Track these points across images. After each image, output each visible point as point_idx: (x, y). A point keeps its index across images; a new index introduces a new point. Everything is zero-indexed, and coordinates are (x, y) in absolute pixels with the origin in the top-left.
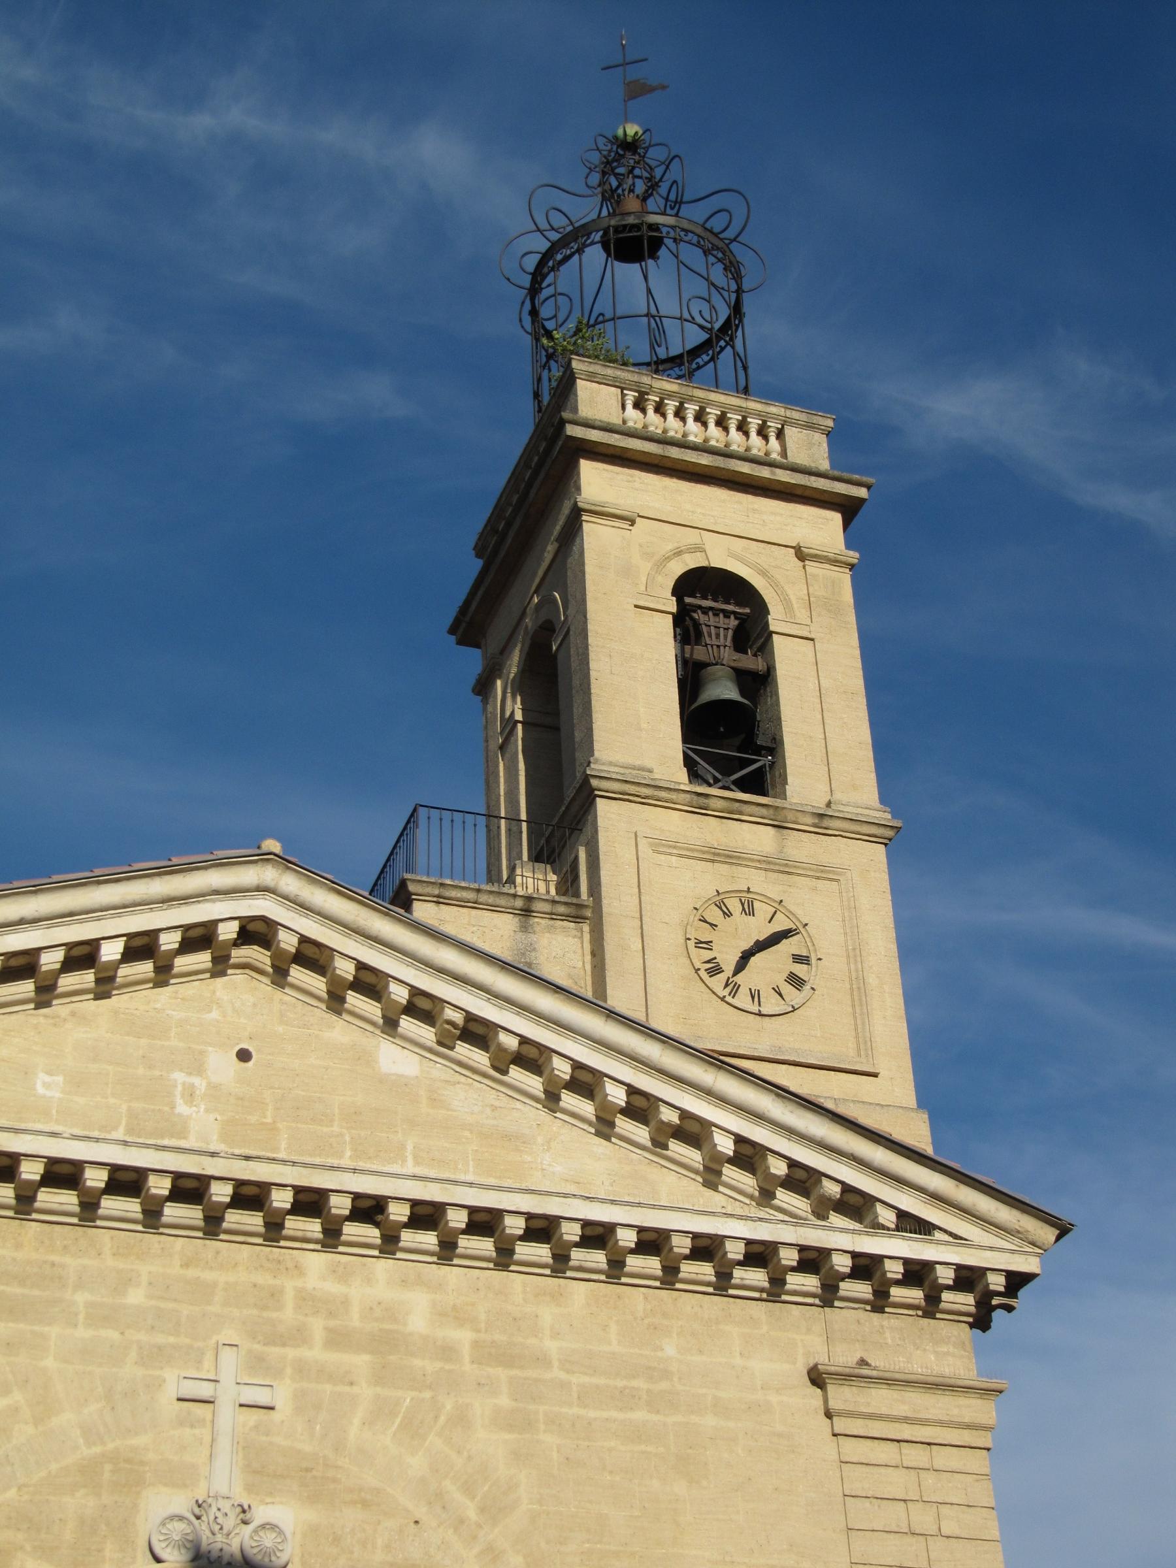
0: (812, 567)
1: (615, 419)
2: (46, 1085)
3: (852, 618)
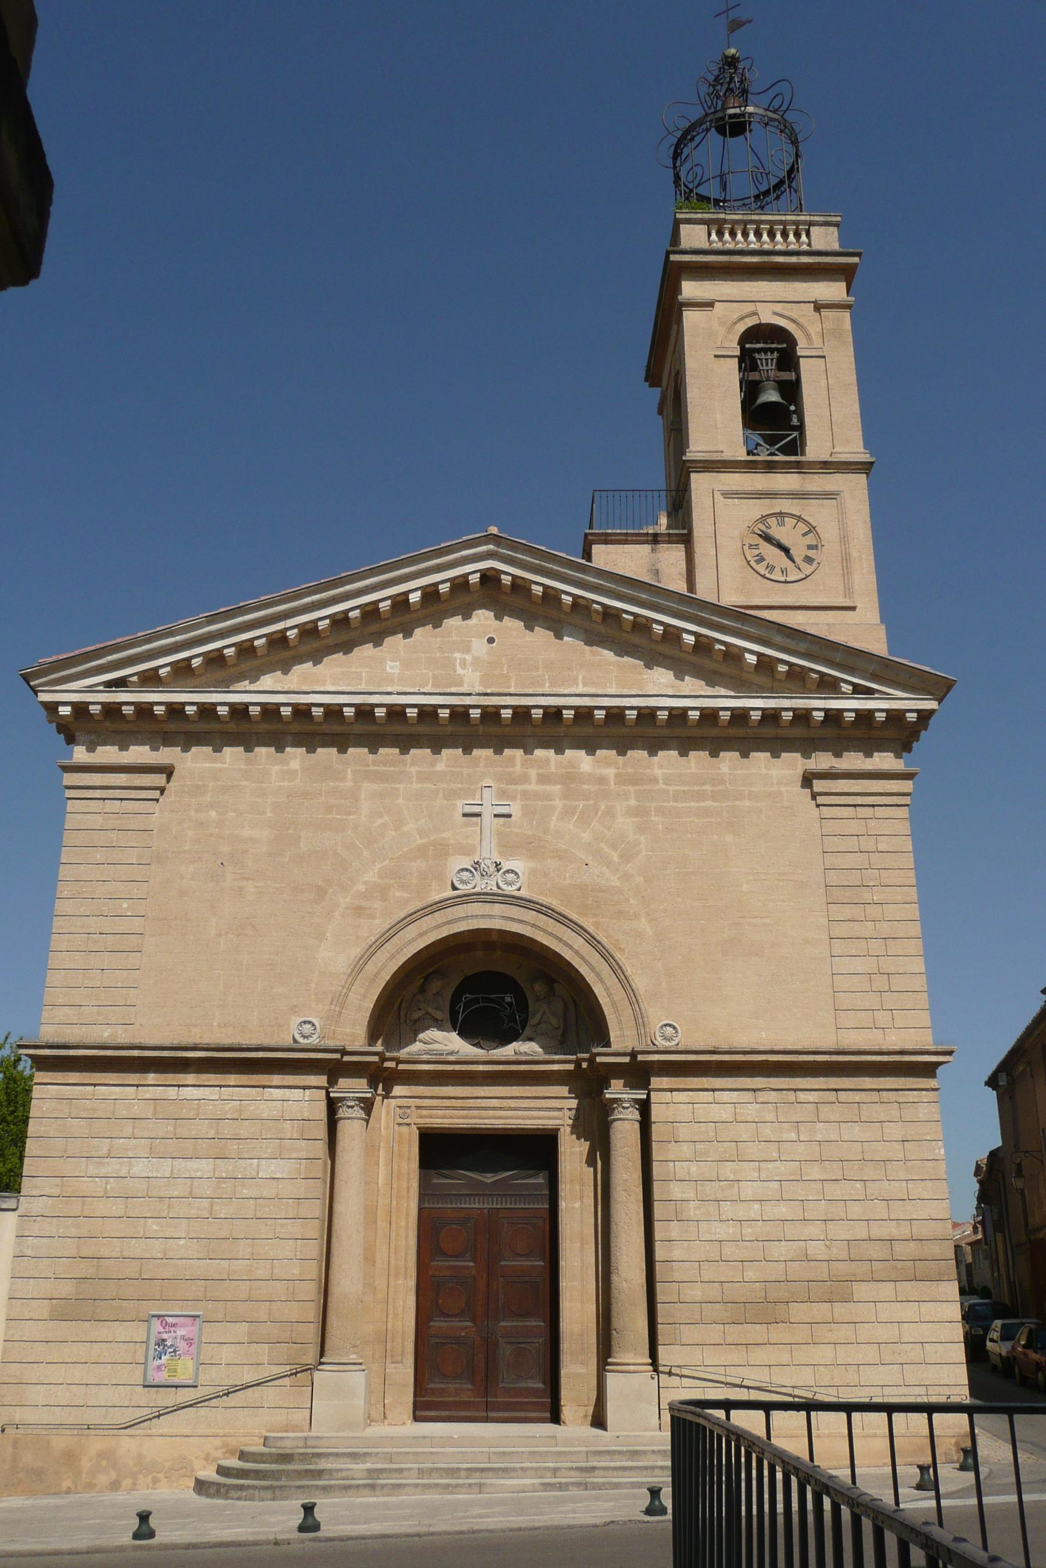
0: (825, 313)
1: (704, 245)
2: (392, 668)
3: (850, 338)
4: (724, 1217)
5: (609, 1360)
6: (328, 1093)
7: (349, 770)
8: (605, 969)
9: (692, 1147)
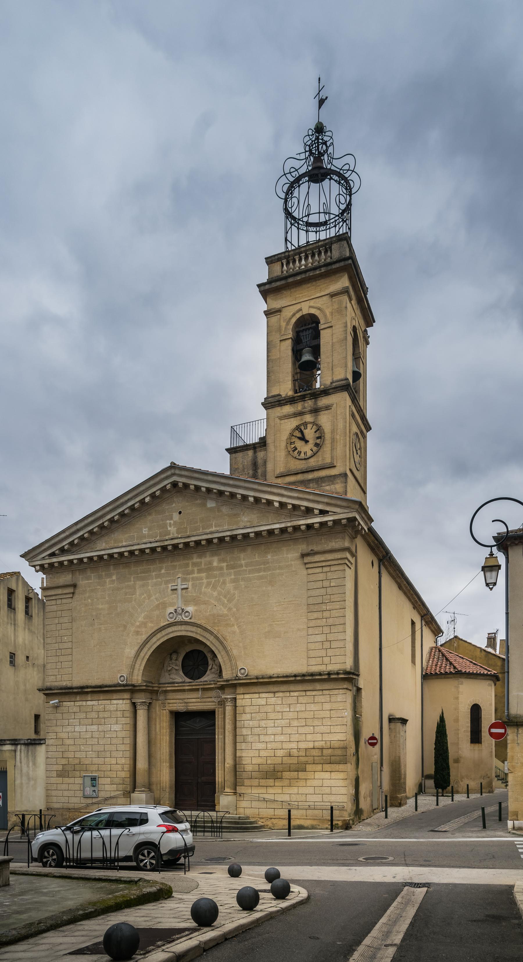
4: (261, 741)
8: (221, 648)
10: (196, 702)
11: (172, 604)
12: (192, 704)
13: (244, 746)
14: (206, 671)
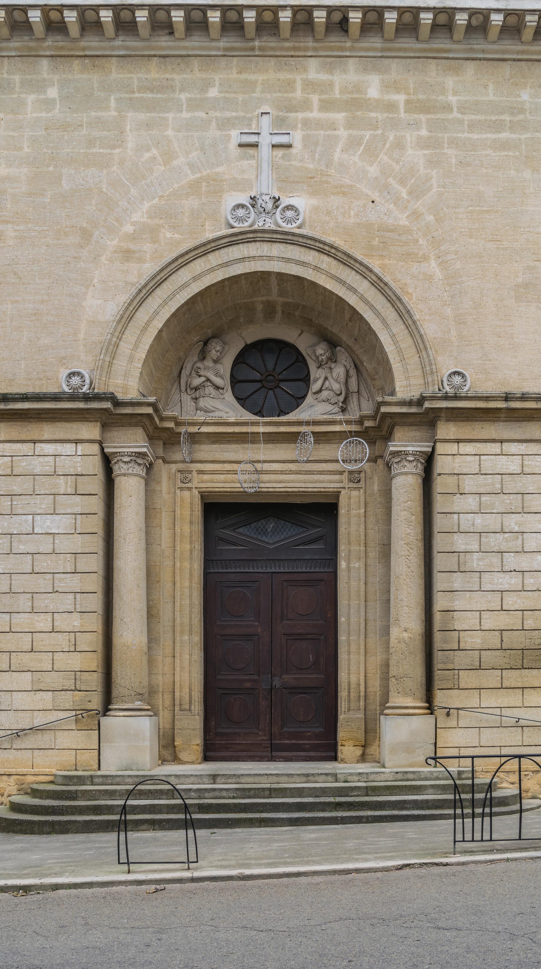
4: (506, 568)
5: (387, 705)
6: (102, 449)
7: (112, 98)
8: (390, 314)
9: (478, 499)
10: (282, 472)
11: (238, 185)
12: (273, 477)
13: (458, 581)
14: (304, 397)
